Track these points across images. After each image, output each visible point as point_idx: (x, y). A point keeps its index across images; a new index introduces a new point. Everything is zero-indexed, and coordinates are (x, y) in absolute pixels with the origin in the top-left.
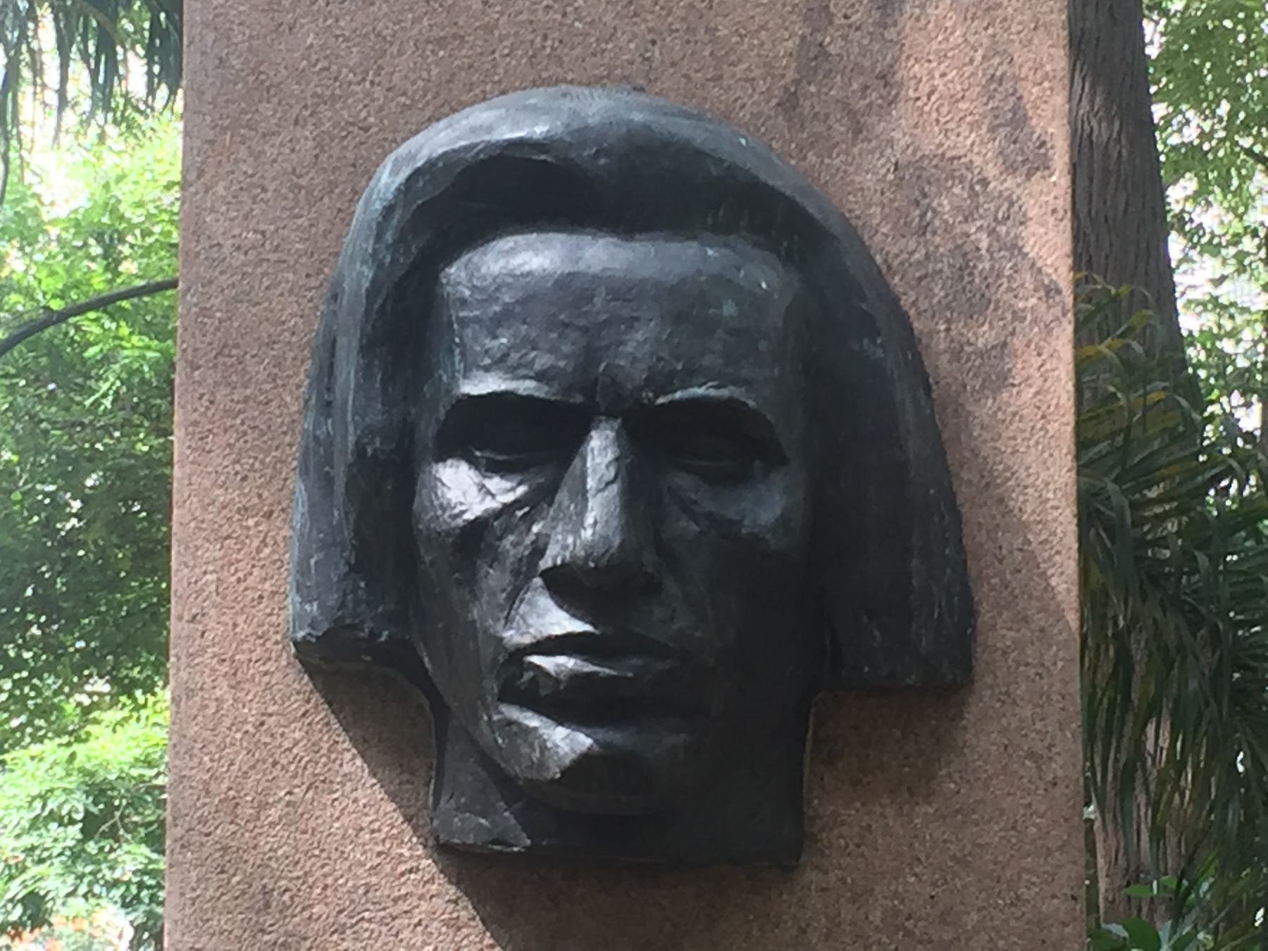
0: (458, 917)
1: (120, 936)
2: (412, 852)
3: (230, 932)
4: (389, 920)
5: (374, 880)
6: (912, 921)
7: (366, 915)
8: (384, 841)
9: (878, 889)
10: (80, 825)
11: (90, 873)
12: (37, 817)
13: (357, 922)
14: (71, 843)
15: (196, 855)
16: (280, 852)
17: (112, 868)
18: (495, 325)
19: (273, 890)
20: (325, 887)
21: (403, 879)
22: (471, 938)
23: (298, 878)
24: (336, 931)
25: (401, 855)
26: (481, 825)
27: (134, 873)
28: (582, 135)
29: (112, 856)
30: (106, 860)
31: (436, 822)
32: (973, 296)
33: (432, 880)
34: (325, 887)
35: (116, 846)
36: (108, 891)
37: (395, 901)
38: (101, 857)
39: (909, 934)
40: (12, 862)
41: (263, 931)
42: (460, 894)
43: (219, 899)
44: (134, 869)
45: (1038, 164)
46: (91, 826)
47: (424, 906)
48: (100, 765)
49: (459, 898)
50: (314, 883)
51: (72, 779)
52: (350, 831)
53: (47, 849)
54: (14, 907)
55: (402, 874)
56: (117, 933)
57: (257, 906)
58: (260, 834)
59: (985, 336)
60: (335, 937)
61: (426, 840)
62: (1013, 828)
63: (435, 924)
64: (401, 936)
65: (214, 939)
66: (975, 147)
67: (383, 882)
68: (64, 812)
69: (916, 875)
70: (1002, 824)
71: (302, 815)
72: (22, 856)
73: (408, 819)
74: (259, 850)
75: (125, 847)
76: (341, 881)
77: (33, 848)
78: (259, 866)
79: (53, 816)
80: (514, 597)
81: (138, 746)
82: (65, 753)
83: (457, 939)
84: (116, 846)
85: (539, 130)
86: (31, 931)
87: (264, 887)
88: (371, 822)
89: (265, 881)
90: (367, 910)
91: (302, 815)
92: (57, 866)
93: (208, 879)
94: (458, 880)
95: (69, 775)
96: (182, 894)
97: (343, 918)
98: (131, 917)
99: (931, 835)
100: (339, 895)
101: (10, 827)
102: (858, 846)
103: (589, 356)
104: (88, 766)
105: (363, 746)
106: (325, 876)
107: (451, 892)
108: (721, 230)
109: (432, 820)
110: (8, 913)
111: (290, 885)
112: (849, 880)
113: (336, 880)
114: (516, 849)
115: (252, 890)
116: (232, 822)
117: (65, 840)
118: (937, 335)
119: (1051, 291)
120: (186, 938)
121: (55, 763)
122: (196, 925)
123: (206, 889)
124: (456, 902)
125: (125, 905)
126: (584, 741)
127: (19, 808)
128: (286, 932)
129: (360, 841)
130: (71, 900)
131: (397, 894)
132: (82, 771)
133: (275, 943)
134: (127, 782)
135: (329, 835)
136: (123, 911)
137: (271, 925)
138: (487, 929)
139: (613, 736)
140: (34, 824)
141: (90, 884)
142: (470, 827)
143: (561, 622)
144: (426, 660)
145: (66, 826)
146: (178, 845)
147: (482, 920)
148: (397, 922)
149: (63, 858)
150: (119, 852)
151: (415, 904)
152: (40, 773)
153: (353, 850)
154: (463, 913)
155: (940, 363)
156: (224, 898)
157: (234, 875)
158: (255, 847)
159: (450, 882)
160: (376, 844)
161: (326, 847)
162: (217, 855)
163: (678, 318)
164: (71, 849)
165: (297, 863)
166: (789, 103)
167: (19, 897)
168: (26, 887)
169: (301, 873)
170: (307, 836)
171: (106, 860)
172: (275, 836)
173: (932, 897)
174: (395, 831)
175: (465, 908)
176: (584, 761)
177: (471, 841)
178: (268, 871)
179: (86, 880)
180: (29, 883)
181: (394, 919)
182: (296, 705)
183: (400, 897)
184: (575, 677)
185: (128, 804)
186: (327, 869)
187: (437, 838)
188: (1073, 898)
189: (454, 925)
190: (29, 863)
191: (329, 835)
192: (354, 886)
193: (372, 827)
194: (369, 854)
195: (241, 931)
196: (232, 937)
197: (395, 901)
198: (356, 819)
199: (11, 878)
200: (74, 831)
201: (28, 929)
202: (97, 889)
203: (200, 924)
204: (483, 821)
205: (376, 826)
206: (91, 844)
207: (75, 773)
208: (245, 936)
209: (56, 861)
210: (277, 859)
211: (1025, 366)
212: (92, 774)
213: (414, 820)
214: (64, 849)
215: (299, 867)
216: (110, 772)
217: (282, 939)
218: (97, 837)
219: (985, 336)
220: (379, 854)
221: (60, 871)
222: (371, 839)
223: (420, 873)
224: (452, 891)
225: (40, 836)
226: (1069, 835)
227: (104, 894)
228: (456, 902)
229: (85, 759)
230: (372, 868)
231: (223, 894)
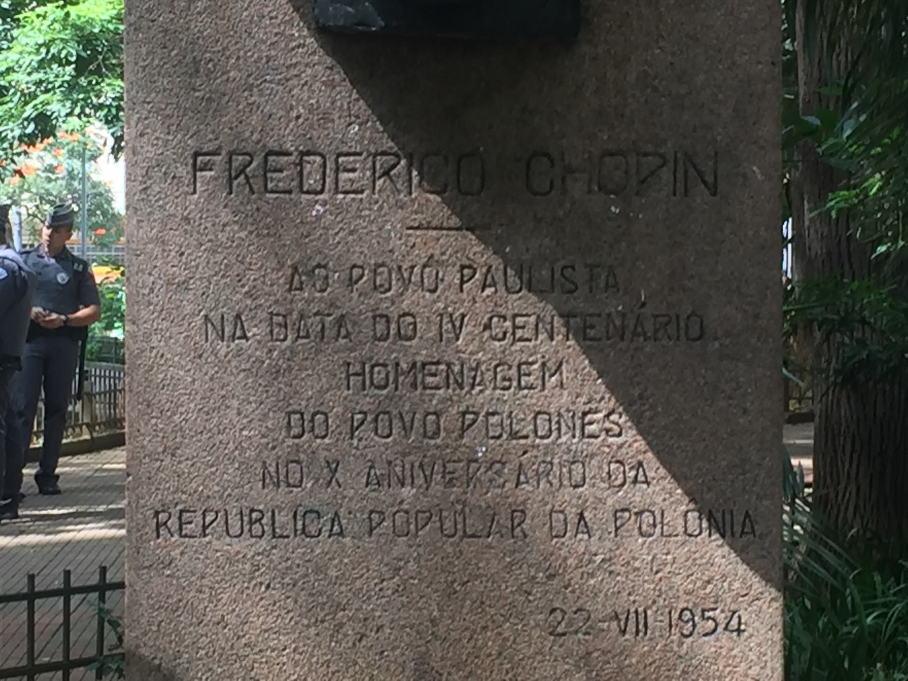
0: (334, 79)
1: (105, 144)
3: (171, 90)
4: (284, 81)
5: (273, 53)
6: (657, 81)
7: (268, 77)
8: (279, 25)
9: (633, 58)
10: (73, 66)
11: (82, 99)
12: (43, 60)
13: (261, 83)
14: (67, 78)
15: (145, 36)
16: (205, 34)
17: (98, 97)
19: (201, 60)
20: (238, 58)
21: (294, 52)
22: (343, 94)
23: (219, 51)
24: (246, 90)
25: (293, 35)
26: (348, 12)
27: (113, 99)
29: (98, 87)
30: (93, 90)
31: (316, 12)
33: (314, 53)
34: (238, 58)
35: (100, 80)
36: (96, 112)
37: (288, 67)
38: (89, 88)
39: (655, 89)
40: (26, 91)
41: (194, 90)
42: (334, 63)
43: (162, 66)
44: (113, 96)
46: (82, 66)
47: (309, 71)
48: (87, 21)
49: (333, 66)
50: (230, 55)
51: (67, 32)
52: (255, 18)
53: (51, 83)
54: (29, 124)
55: (293, 49)
56: (102, 142)
57: (190, 72)
58: (190, 20)
60: (246, 94)
61: (310, 24)
62: (732, 14)
63: (318, 84)
64: (292, 93)
65: (160, 95)
67: (279, 55)
68: (62, 56)
69: (660, 48)
70: (723, 12)
71: (221, 7)
72: (33, 88)
73: (297, 9)
74: (190, 31)
75: (107, 81)
76: (249, 54)
77: (41, 82)
78: (191, 43)
79: (56, 59)
81: (114, 8)
82: (60, 14)
83: (333, 95)
84: (100, 80)
86: (42, 142)
87: (194, 58)
88: (270, 12)
89: (195, 54)
90: (268, 74)
91: (221, 7)
92: (58, 96)
93: (154, 53)
94: (333, 52)
95: (65, 29)
96: (136, 64)
97: (251, 80)
98: (112, 131)
99: (672, 20)
100: (249, 64)
101: (24, 67)
102: (620, 27)
104: (78, 23)
106: (239, 50)
107: (329, 61)
109: (313, 9)
110: (25, 128)
111: (213, 57)
112: (613, 52)
113: (246, 53)
114: (374, 29)
115: (185, 61)
116: (170, 12)
117: (63, 76)
120: (139, 95)
121: (55, 21)
122: (147, 86)
123: (153, 60)
124: (331, 68)
125: (107, 122)
127: (30, 53)
128: (210, 90)
129: (263, 25)
130: (69, 119)
131: (289, 62)
132: (74, 26)
133: (203, 98)
134: (107, 35)
135: (240, 21)
136: (106, 127)
137: (200, 85)
138: (354, 88)
140: (42, 65)
141: (82, 108)
145: (64, 66)
146: (132, 28)
147: (350, 81)
148: (291, 82)
149: (62, 89)
150: (102, 84)
151: (303, 69)
152: (44, 28)
153: (257, 32)
154: (336, 77)
156: (166, 66)
157: (173, 49)
158: (188, 29)
159: (328, 54)
160: (275, 28)
161: (238, 29)
162: (160, 35)
164: (67, 82)
165: (218, 41)
167: (33, 116)
168: (37, 109)
169: (220, 48)
170: (225, 22)
171: (93, 90)
172: (201, 22)
173: (672, 64)
174: (287, 18)
175: (339, 72)
177: (341, 23)
178: (197, 47)
179: (79, 105)
180: (39, 106)
181: (287, 80)
183: (291, 65)
185: (108, 50)
186: (238, 46)
187: (317, 23)
188: (773, 63)
190: (38, 92)
191: (240, 21)
192: (258, 57)
193: (271, 15)
194: (269, 35)
195: (178, 90)
196: (172, 93)
197: (288, 67)
198: (260, 9)
199: (26, 103)
200: (70, 69)
201: (39, 139)
202: (87, 111)
203: (149, 84)
204: (350, 9)
205: (274, 14)
206: (83, 78)
207: (69, 28)
208: (182, 93)
209: (58, 91)
210: (203, 39)
212: (81, 29)
213: (301, 10)
214: (63, 82)
215: (219, 44)
216: (94, 27)
217: (208, 96)
218: (86, 74)
220: (276, 34)
221: (59, 98)
222: (271, 24)
223: (306, 49)
224: (329, 61)
225: (46, 73)
226: (771, 19)
227: (92, 114)
228: (331, 68)
229: (76, 18)
230: (273, 44)
231: (165, 63)
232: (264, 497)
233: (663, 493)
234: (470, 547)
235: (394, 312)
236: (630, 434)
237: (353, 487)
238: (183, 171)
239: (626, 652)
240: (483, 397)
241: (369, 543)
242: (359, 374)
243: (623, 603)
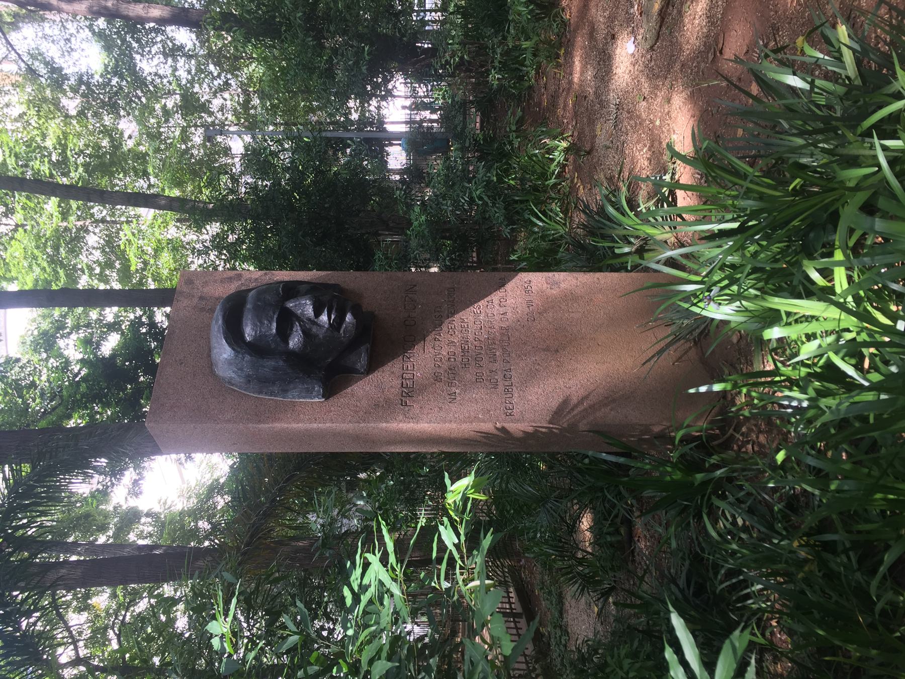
119: (266, 274)
142: (362, 361)
182: (336, 400)
189: (383, 371)
232: (501, 388)
233: (496, 297)
234: (512, 339)
235: (447, 357)
236: (480, 303)
237: (497, 366)
238: (407, 408)
239: (537, 305)
240: (471, 337)
241: (512, 362)
242: (465, 366)
243: (525, 305)
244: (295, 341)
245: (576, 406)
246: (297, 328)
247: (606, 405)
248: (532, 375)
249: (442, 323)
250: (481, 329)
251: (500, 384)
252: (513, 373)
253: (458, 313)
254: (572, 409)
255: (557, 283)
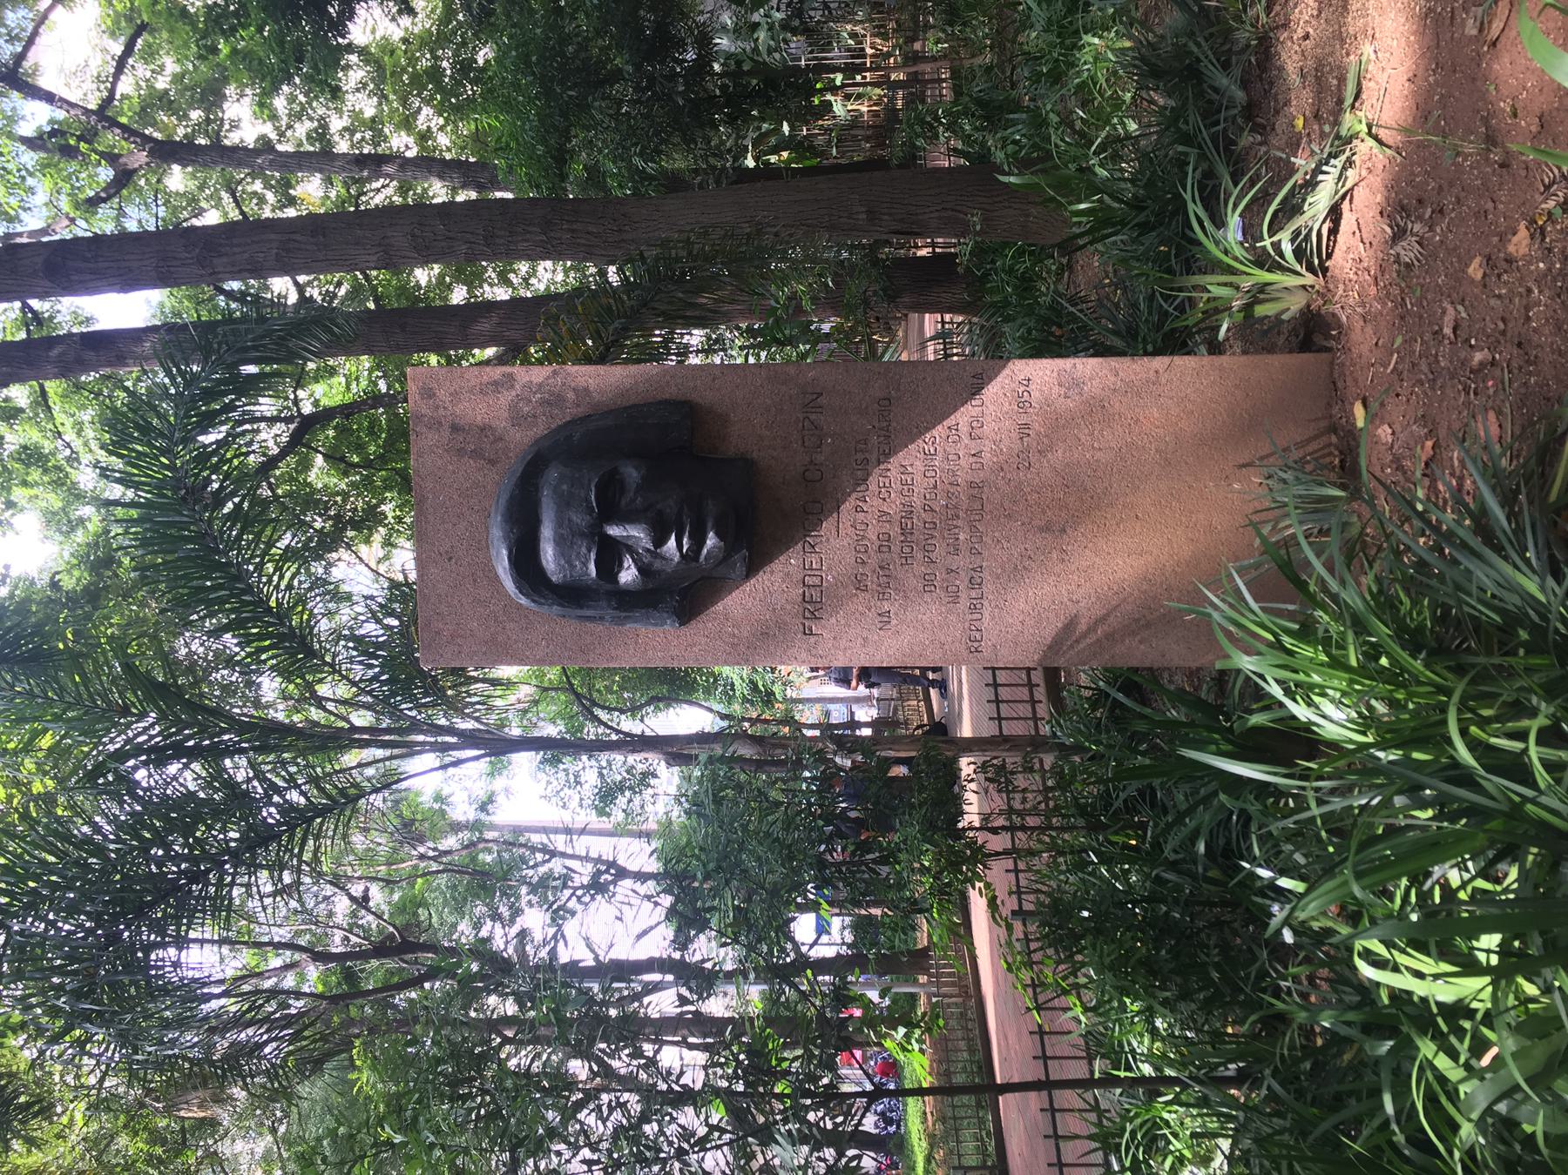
2: (747, 587)
18: (573, 567)
28: (506, 538)
32: (554, 400)
45: (511, 377)
59: (571, 395)
66: (506, 398)
80: (664, 558)
85: (505, 552)
94: (757, 571)
103: (582, 535)
105: (714, 603)
108: (537, 489)
118: (570, 413)
119: (555, 373)
126: (711, 534)
139: (710, 525)
142: (740, 568)
143: (672, 542)
144: (499, 195)
155: (581, 411)
163: (568, 505)
166: (492, 462)
176: (717, 534)
182: (700, 626)
184: (690, 538)
189: (772, 572)
211: (581, 382)
219: (571, 395)
232: (964, 602)
233: (963, 417)
234: (988, 507)
236: (935, 432)
238: (812, 639)
241: (986, 554)
243: (1014, 435)
244: (628, 575)
245: (1084, 635)
246: (628, 561)
247: (1133, 633)
248: (1016, 573)
249: (869, 475)
250: (935, 487)
251: (963, 595)
252: (986, 603)
253: (896, 453)
254: (1077, 641)
255: (1077, 384)
